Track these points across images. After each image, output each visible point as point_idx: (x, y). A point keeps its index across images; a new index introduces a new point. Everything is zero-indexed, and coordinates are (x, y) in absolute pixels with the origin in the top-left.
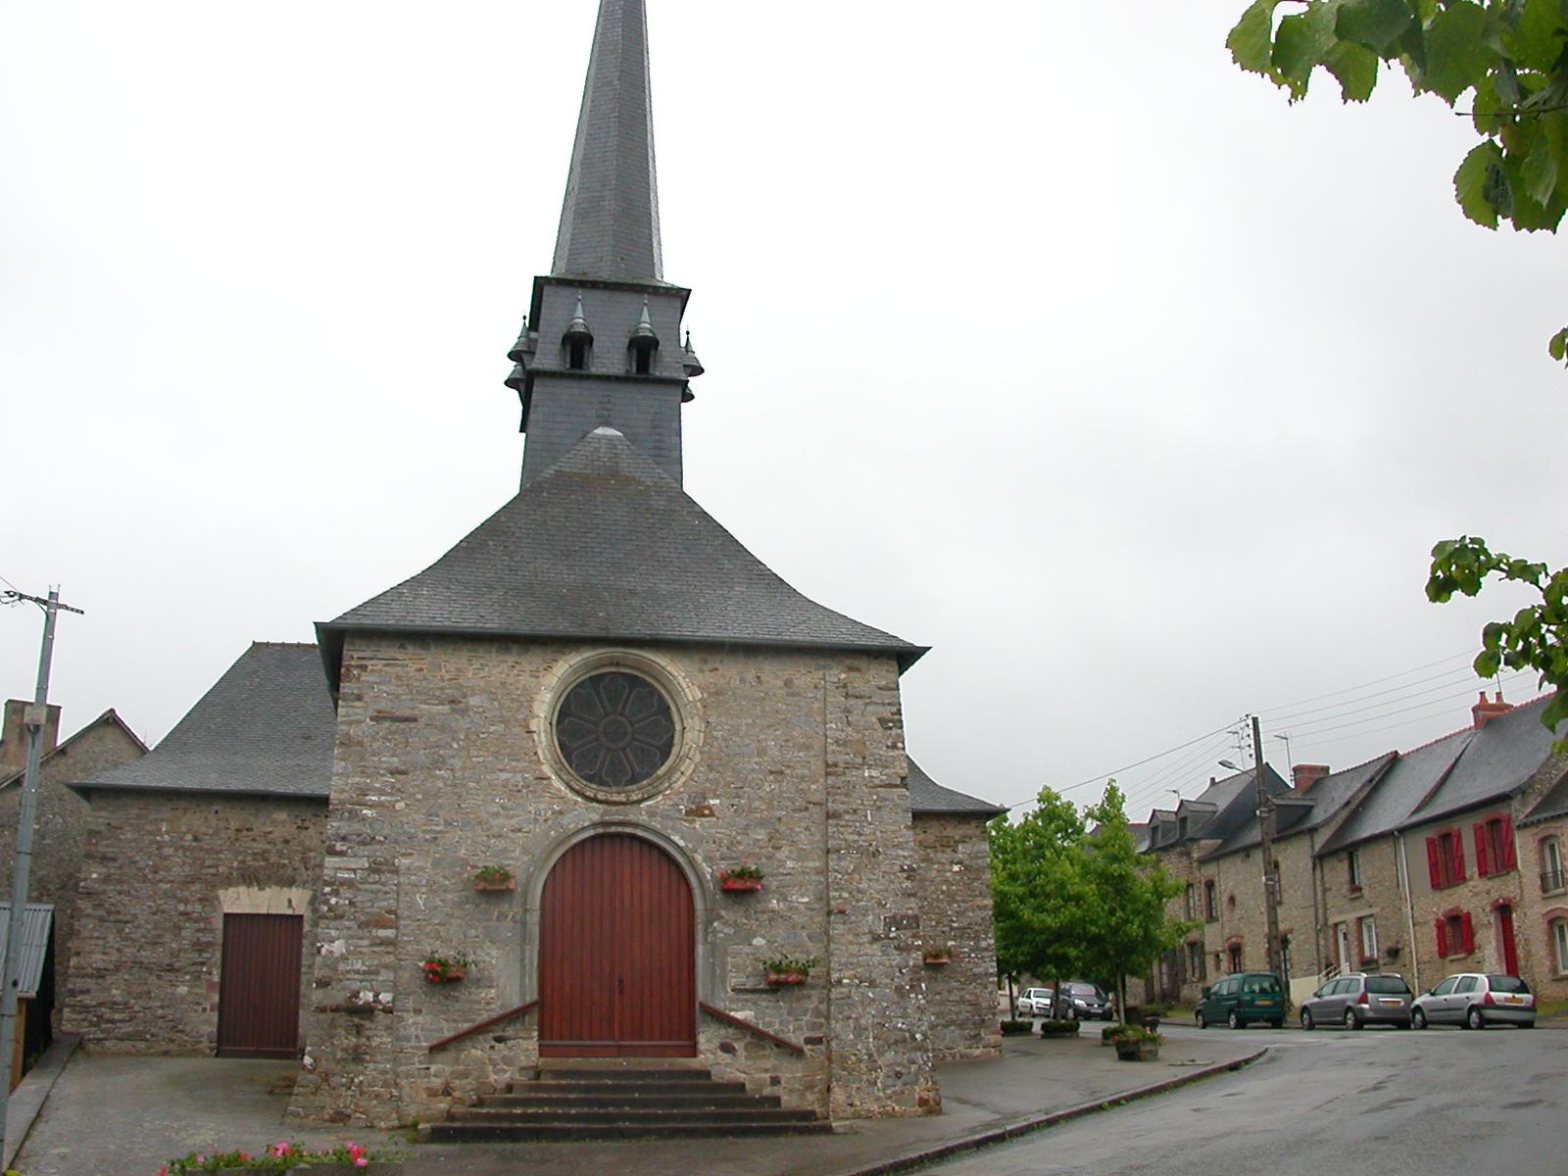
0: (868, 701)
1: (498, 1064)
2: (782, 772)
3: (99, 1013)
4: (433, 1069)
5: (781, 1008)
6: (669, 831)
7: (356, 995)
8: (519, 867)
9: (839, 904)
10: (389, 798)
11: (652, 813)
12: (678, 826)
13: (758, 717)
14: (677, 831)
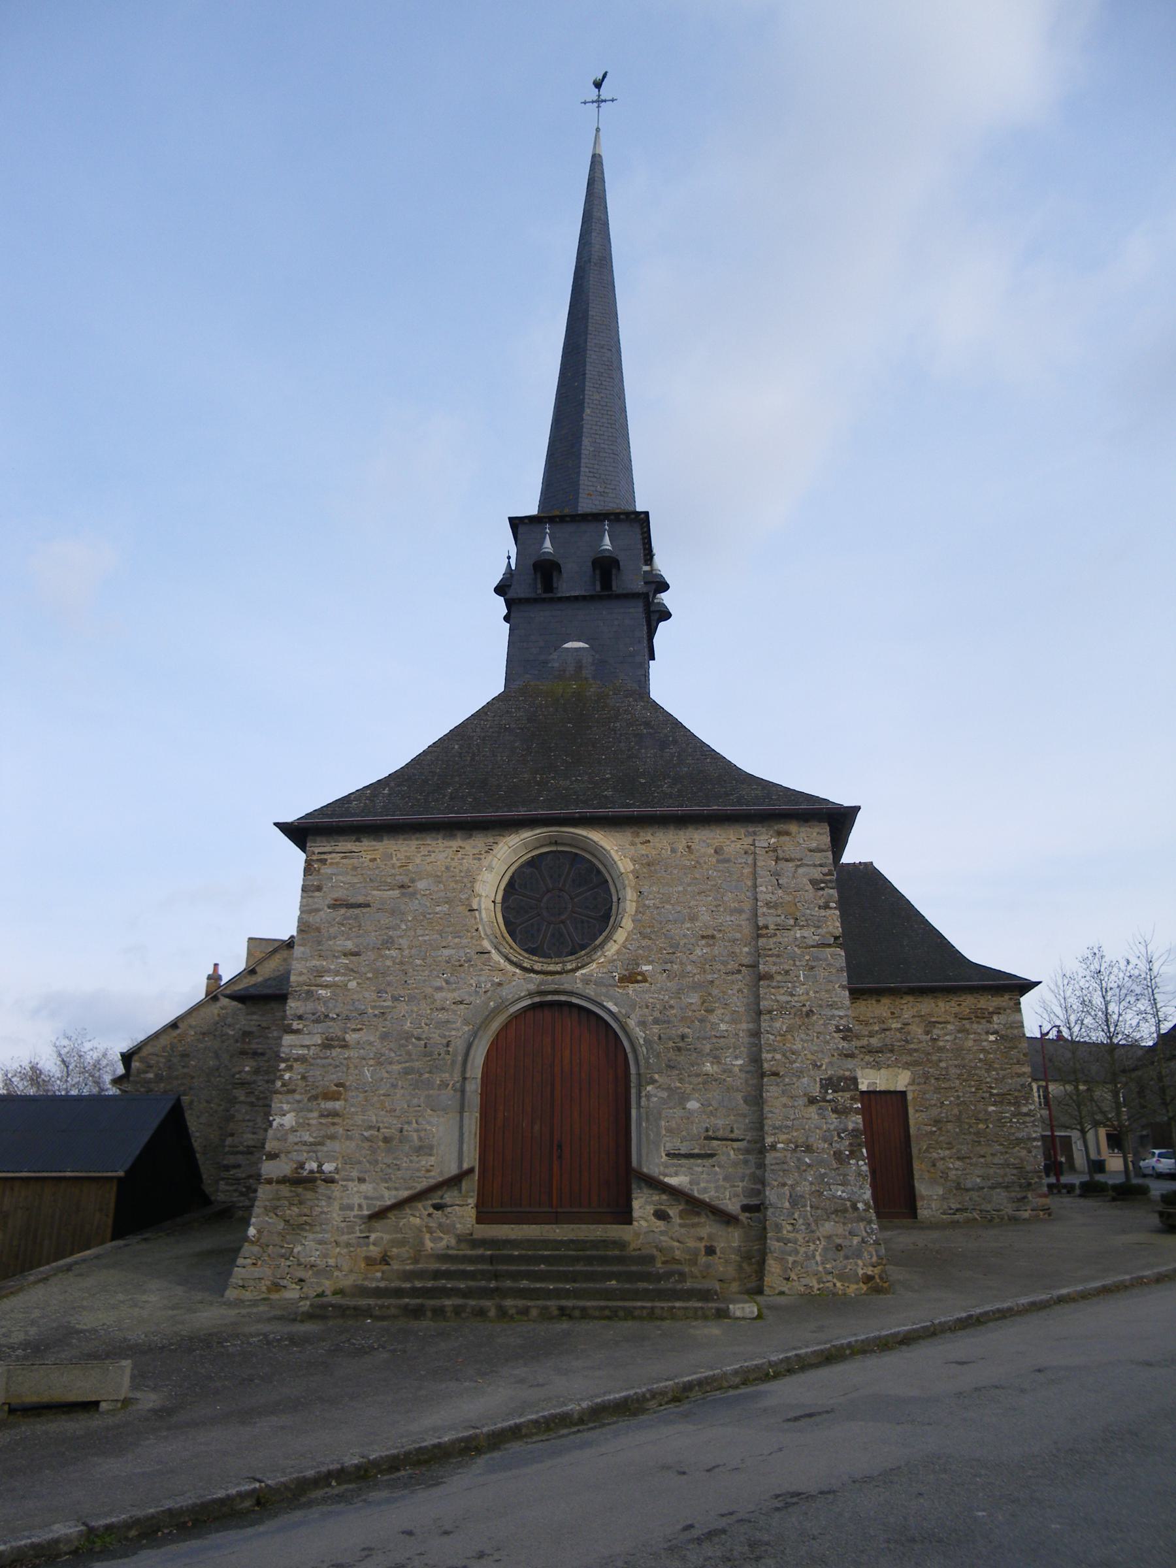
0: (799, 863)
1: (435, 1232)
2: (713, 937)
3: (248, 1184)
4: (373, 1236)
5: (716, 1173)
6: (603, 998)
7: (301, 1166)
8: (460, 1037)
9: (773, 1065)
10: (342, 978)
11: (586, 981)
12: (611, 992)
13: (689, 885)
14: (611, 998)
